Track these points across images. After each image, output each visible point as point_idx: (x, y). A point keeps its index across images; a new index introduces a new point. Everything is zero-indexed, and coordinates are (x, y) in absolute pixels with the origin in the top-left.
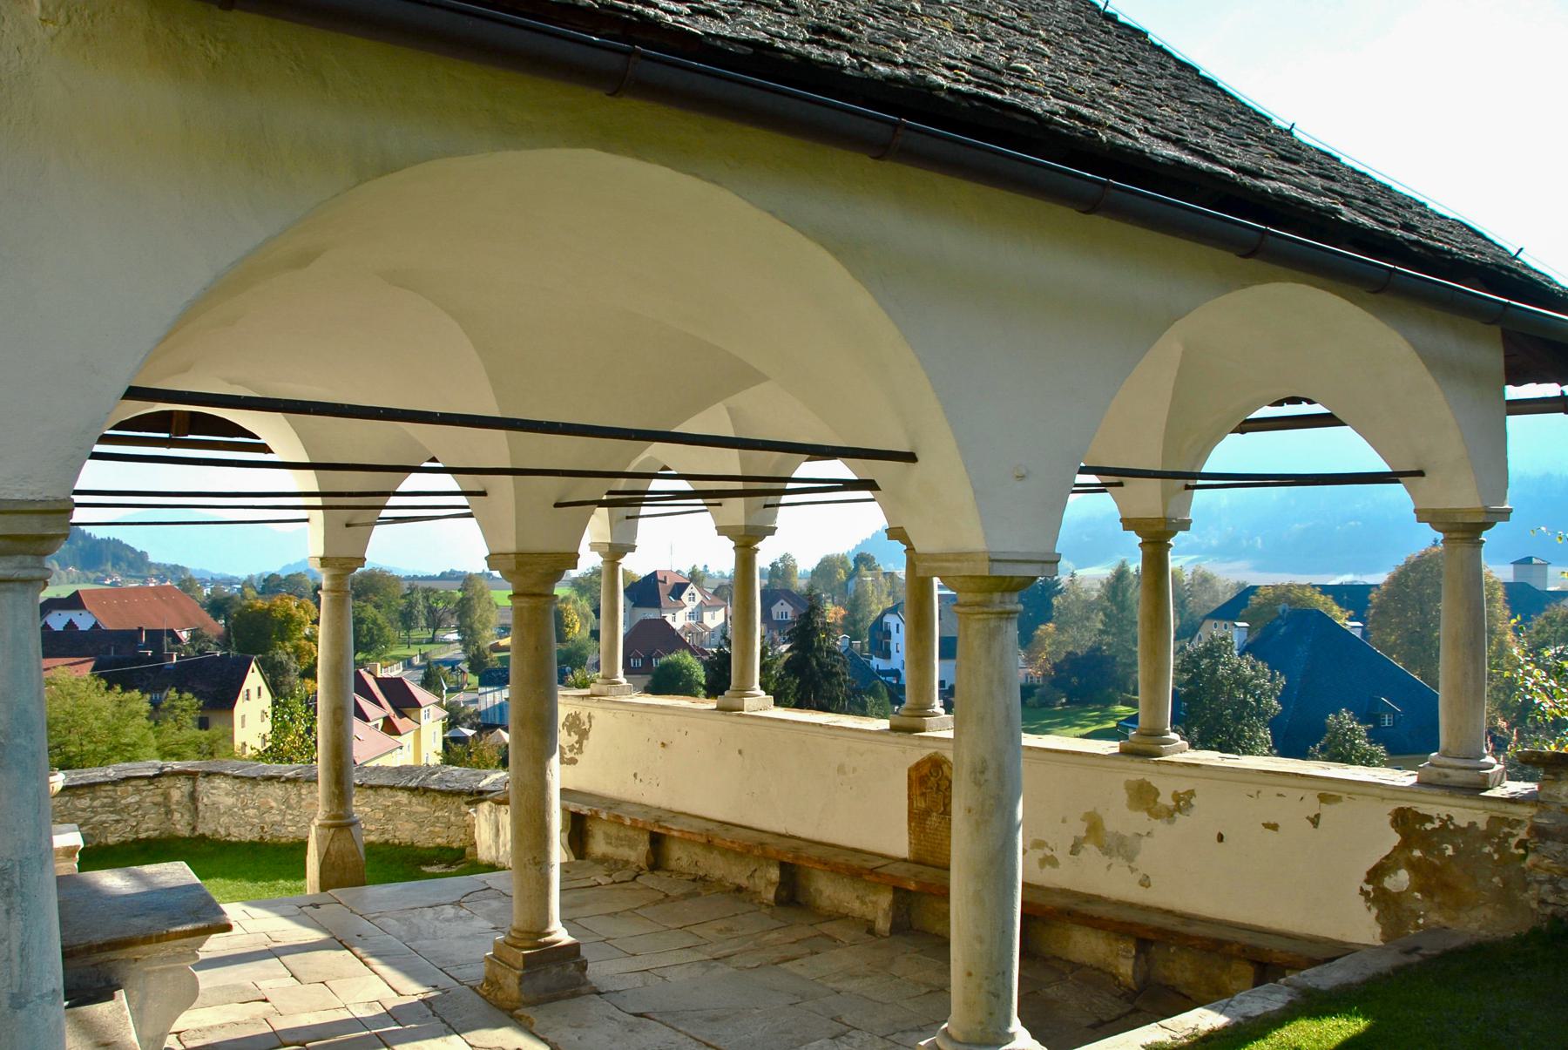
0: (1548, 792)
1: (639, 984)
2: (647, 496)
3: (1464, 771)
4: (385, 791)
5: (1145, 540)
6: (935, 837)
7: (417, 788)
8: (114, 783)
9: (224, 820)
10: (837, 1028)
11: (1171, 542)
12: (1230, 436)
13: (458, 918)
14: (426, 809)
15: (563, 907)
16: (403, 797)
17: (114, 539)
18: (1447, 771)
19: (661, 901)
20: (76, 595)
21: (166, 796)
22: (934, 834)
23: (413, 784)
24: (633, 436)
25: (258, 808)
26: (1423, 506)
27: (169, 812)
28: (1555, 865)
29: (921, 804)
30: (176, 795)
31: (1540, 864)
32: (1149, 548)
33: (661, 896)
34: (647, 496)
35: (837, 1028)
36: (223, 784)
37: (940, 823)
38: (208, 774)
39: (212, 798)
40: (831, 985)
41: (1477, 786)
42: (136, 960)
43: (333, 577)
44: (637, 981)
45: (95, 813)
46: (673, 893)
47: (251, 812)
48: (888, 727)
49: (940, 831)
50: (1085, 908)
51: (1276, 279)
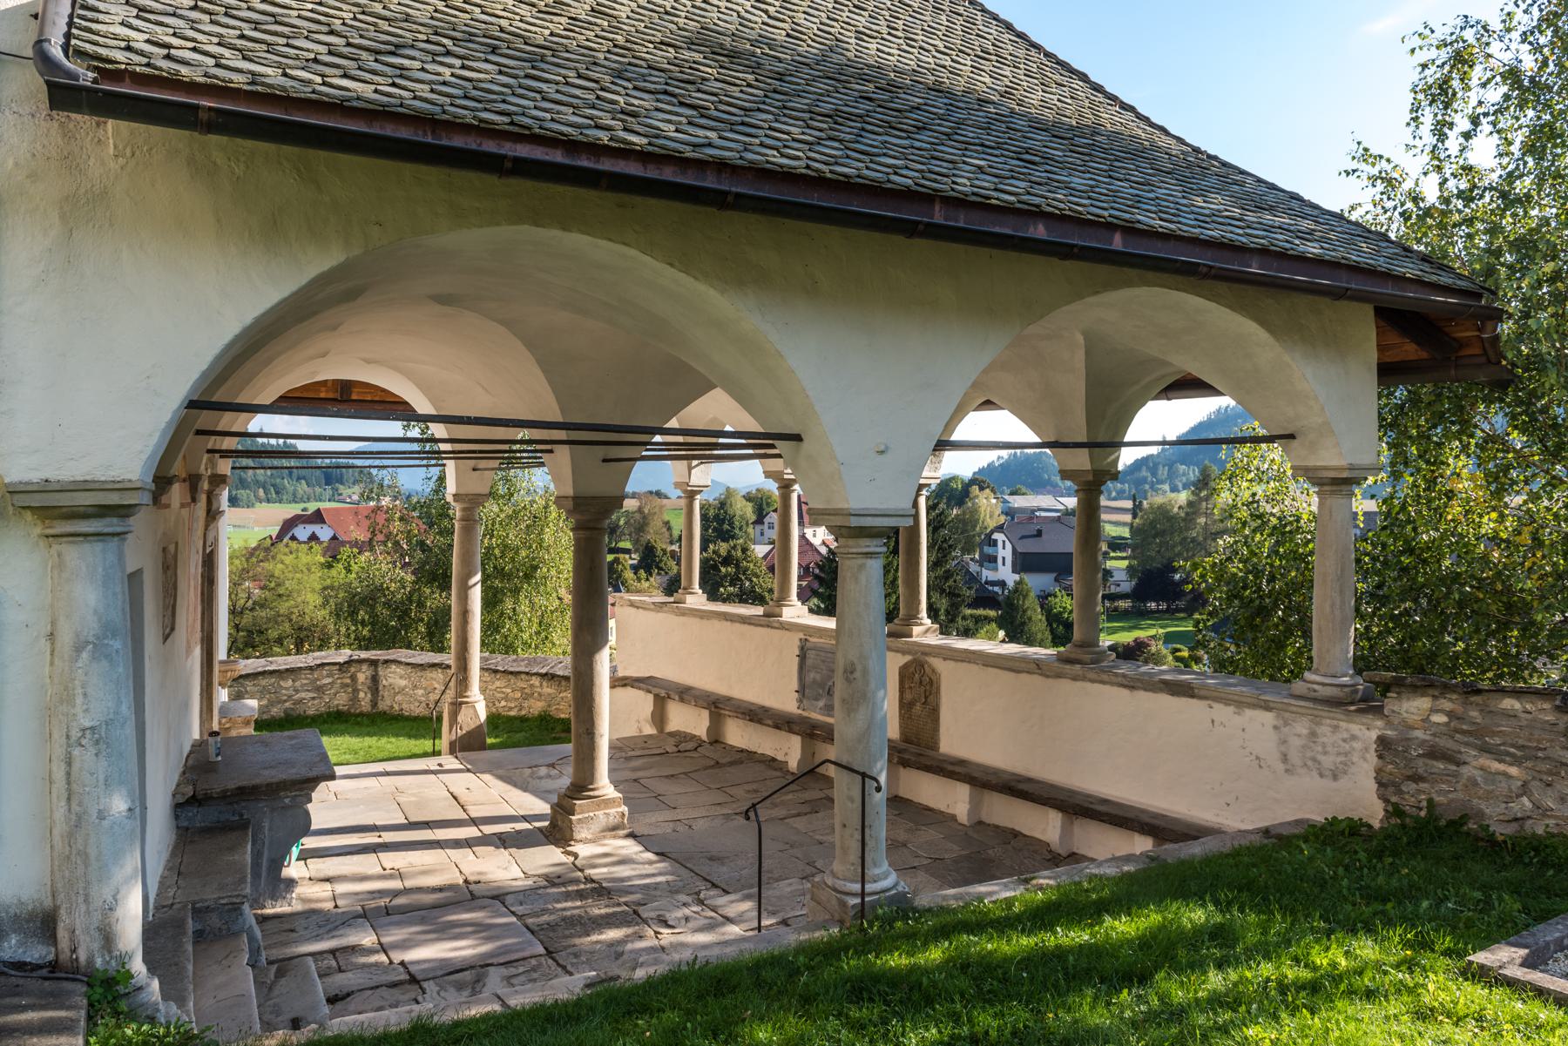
1: (669, 831)
2: (721, 440)
4: (523, 676)
7: (546, 674)
8: (311, 668)
9: (398, 698)
10: (809, 870)
13: (549, 776)
15: (611, 771)
16: (535, 681)
18: (1316, 687)
19: (712, 767)
20: (318, 511)
21: (354, 678)
23: (543, 671)
24: (1076, 250)
25: (425, 689)
27: (356, 691)
29: (908, 696)
30: (361, 677)
33: (712, 763)
34: (721, 440)
35: (809, 870)
36: (400, 670)
38: (386, 662)
39: (390, 680)
40: (817, 837)
42: (1465, 763)
43: (464, 510)
44: (668, 828)
45: (297, 691)
46: (722, 761)
47: (420, 692)
50: (1021, 786)
51: (1129, 284)
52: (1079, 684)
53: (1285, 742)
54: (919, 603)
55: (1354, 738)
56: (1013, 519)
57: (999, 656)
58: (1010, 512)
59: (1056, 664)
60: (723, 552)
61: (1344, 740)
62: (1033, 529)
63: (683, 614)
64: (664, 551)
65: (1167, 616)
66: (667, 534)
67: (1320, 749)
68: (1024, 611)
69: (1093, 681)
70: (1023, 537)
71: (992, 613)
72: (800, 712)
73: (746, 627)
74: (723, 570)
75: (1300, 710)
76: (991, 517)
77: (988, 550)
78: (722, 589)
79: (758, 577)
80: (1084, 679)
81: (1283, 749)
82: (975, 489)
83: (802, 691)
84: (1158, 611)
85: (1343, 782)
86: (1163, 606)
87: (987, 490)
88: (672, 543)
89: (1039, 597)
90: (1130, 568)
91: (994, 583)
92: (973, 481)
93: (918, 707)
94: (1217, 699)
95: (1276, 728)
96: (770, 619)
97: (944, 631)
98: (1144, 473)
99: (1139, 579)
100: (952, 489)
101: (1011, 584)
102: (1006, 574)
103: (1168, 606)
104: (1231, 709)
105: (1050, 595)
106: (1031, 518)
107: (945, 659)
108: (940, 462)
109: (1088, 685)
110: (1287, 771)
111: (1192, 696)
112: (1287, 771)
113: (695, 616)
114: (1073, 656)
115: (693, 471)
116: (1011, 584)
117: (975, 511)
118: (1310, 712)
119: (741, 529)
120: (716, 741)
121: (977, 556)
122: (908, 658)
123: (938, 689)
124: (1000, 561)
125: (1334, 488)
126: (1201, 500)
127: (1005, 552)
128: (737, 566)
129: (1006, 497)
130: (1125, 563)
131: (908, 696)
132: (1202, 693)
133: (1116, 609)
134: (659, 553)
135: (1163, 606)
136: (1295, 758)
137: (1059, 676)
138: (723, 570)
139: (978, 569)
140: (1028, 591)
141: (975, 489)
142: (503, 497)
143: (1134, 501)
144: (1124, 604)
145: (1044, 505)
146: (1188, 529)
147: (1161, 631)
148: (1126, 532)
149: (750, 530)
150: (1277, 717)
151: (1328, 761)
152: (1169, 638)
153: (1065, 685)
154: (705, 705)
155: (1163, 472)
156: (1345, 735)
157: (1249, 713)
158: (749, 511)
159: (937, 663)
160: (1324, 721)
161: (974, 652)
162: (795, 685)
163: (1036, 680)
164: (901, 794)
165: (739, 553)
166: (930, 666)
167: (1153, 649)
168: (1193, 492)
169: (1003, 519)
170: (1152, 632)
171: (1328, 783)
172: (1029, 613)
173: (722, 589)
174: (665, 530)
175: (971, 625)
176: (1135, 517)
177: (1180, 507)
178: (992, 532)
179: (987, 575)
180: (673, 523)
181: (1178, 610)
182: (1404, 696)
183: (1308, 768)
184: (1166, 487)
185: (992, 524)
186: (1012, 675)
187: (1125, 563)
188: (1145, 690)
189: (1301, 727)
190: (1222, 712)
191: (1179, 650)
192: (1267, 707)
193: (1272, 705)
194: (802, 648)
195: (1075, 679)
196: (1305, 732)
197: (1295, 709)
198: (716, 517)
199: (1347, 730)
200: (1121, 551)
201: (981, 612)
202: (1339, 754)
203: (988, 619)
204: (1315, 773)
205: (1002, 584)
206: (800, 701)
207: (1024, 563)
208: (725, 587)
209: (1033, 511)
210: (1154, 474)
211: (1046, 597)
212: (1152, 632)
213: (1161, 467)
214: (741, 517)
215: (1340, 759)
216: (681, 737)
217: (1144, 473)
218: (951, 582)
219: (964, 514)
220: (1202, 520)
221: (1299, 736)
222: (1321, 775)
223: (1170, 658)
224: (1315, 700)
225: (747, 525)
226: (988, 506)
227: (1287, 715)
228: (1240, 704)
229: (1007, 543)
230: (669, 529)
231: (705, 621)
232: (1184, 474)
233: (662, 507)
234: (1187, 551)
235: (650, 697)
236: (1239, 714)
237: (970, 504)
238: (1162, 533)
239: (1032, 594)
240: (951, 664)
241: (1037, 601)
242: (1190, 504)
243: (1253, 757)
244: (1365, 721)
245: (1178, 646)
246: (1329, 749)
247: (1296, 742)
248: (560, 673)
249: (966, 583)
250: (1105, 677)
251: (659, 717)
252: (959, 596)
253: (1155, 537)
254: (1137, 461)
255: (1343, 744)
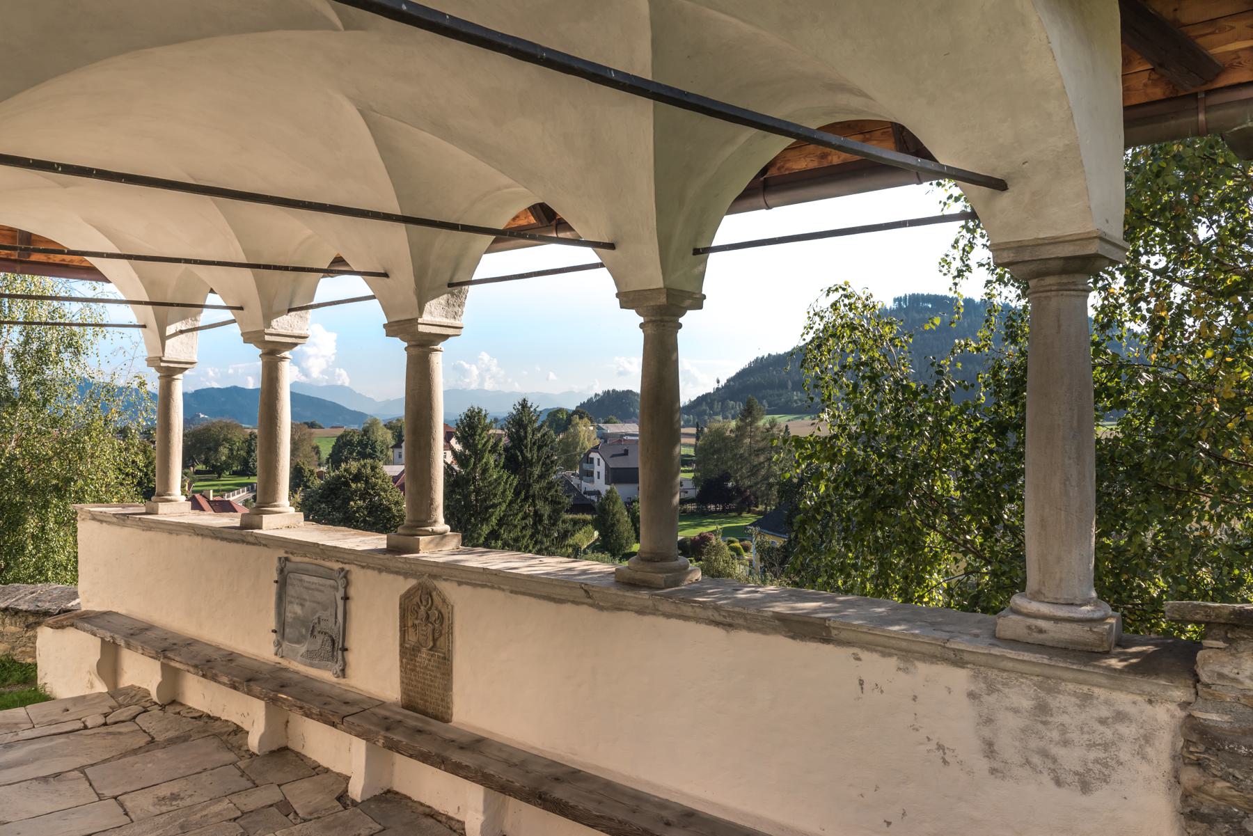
0: (1217, 668)
3: (1068, 625)
5: (673, 318)
6: (425, 676)
11: (681, 320)
12: (726, 218)
14: (18, 629)
17: (680, 326)
22: (424, 673)
26: (1000, 239)
28: (1235, 793)
29: (412, 638)
31: (1208, 787)
32: (267, 358)
37: (430, 660)
41: (1089, 648)
48: (385, 546)
49: (430, 670)
52: (648, 620)
53: (989, 721)
54: (431, 501)
55: (1121, 717)
56: (606, 442)
57: (531, 578)
58: (604, 437)
59: (613, 590)
60: (354, 470)
61: (1103, 721)
62: (620, 450)
63: (150, 529)
64: (312, 472)
65: (722, 515)
66: (316, 457)
67: (1055, 735)
68: (614, 515)
69: (668, 616)
70: (613, 456)
71: (589, 517)
72: (278, 659)
73: (219, 543)
74: (353, 486)
75: (1020, 667)
76: (588, 440)
77: (586, 466)
78: (352, 503)
79: (385, 491)
80: (655, 612)
81: (986, 732)
82: (576, 418)
83: (281, 630)
84: (716, 512)
85: (1101, 796)
86: (720, 508)
87: (586, 419)
88: (320, 465)
89: (626, 503)
90: (695, 478)
91: (591, 493)
92: (575, 412)
93: (424, 654)
94: (868, 646)
95: (972, 695)
96: (246, 533)
97: (469, 541)
98: (704, 407)
99: (702, 487)
100: (559, 419)
101: (604, 493)
102: (600, 484)
103: (724, 507)
104: (893, 662)
105: (634, 501)
106: (620, 441)
107: (460, 583)
108: (461, 305)
109: (661, 621)
110: (993, 771)
111: (827, 640)
112: (993, 771)
113: (163, 530)
114: (638, 576)
115: (168, 342)
116: (604, 493)
117: (576, 435)
118: (1037, 670)
119: (381, 452)
120: (174, 702)
121: (577, 472)
122: (412, 582)
123: (451, 627)
124: (595, 475)
125: (1065, 279)
126: (747, 425)
127: (599, 468)
128: (367, 482)
129: (601, 425)
130: (692, 475)
131: (412, 638)
132: (844, 635)
133: (684, 511)
134: (307, 473)
135: (720, 508)
136: (1008, 747)
137: (618, 607)
138: (353, 486)
139: (579, 482)
140: (617, 498)
141: (576, 418)
142: (35, 403)
143: (697, 427)
144: (691, 507)
145: (630, 431)
146: (737, 447)
147: (719, 527)
148: (691, 452)
149: (390, 453)
150: (975, 677)
151: (1071, 758)
152: (726, 532)
153: (627, 622)
154: (153, 653)
155: (717, 406)
156: (1105, 712)
157: (923, 668)
158: (389, 437)
159: (448, 589)
160: (1063, 686)
161: (497, 573)
162: (272, 623)
163: (585, 613)
164: (396, 788)
165: (369, 471)
166: (440, 594)
167: (714, 542)
168: (740, 419)
169: (598, 442)
170: (713, 528)
171: (1071, 797)
172: (618, 516)
173: (352, 503)
174: (313, 453)
175: (570, 528)
176: (698, 439)
177: (731, 431)
178: (589, 452)
179: (586, 486)
180: (321, 449)
181: (731, 510)
182: (1242, 646)
183: (1034, 768)
184: (720, 418)
185: (589, 445)
186: (551, 606)
187: (692, 475)
188: (750, 629)
189: (1021, 696)
190: (877, 667)
191: (733, 542)
192: (958, 660)
193: (966, 657)
194: (281, 571)
195: (641, 611)
196: (1027, 704)
197: (1010, 665)
198: (360, 442)
199: (1107, 702)
200: (688, 466)
201: (580, 516)
202: (1091, 745)
203: (585, 523)
204: (1046, 779)
205: (598, 493)
206: (278, 644)
207: (616, 476)
208: (355, 502)
209: (622, 436)
210: (711, 408)
211: (631, 503)
212: (713, 528)
213: (716, 403)
214: (382, 442)
215: (1093, 755)
216: (136, 695)
217: (704, 407)
218: (553, 492)
219: (567, 438)
220: (747, 441)
221: (1016, 711)
222: (1058, 782)
223: (727, 548)
224: (1041, 647)
225: (387, 448)
226: (586, 432)
227: (992, 674)
228: (907, 654)
229: (602, 461)
230: (318, 452)
231: (174, 537)
232: (732, 408)
233: (311, 434)
234: (737, 464)
235: (98, 642)
236: (906, 670)
237: (572, 430)
238: (718, 451)
239: (620, 501)
240: (467, 590)
241: (624, 506)
242: (738, 428)
243: (933, 746)
244: (1147, 688)
245: (732, 539)
246: (1074, 736)
247: (1009, 722)
248: (24, 607)
249: (565, 492)
250: (687, 610)
251: (109, 666)
252: (559, 503)
253: (713, 454)
254: (698, 398)
255: (1101, 728)
